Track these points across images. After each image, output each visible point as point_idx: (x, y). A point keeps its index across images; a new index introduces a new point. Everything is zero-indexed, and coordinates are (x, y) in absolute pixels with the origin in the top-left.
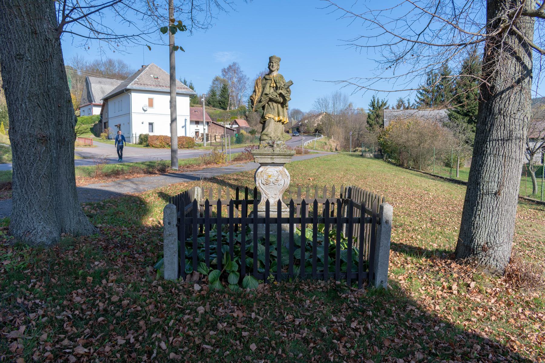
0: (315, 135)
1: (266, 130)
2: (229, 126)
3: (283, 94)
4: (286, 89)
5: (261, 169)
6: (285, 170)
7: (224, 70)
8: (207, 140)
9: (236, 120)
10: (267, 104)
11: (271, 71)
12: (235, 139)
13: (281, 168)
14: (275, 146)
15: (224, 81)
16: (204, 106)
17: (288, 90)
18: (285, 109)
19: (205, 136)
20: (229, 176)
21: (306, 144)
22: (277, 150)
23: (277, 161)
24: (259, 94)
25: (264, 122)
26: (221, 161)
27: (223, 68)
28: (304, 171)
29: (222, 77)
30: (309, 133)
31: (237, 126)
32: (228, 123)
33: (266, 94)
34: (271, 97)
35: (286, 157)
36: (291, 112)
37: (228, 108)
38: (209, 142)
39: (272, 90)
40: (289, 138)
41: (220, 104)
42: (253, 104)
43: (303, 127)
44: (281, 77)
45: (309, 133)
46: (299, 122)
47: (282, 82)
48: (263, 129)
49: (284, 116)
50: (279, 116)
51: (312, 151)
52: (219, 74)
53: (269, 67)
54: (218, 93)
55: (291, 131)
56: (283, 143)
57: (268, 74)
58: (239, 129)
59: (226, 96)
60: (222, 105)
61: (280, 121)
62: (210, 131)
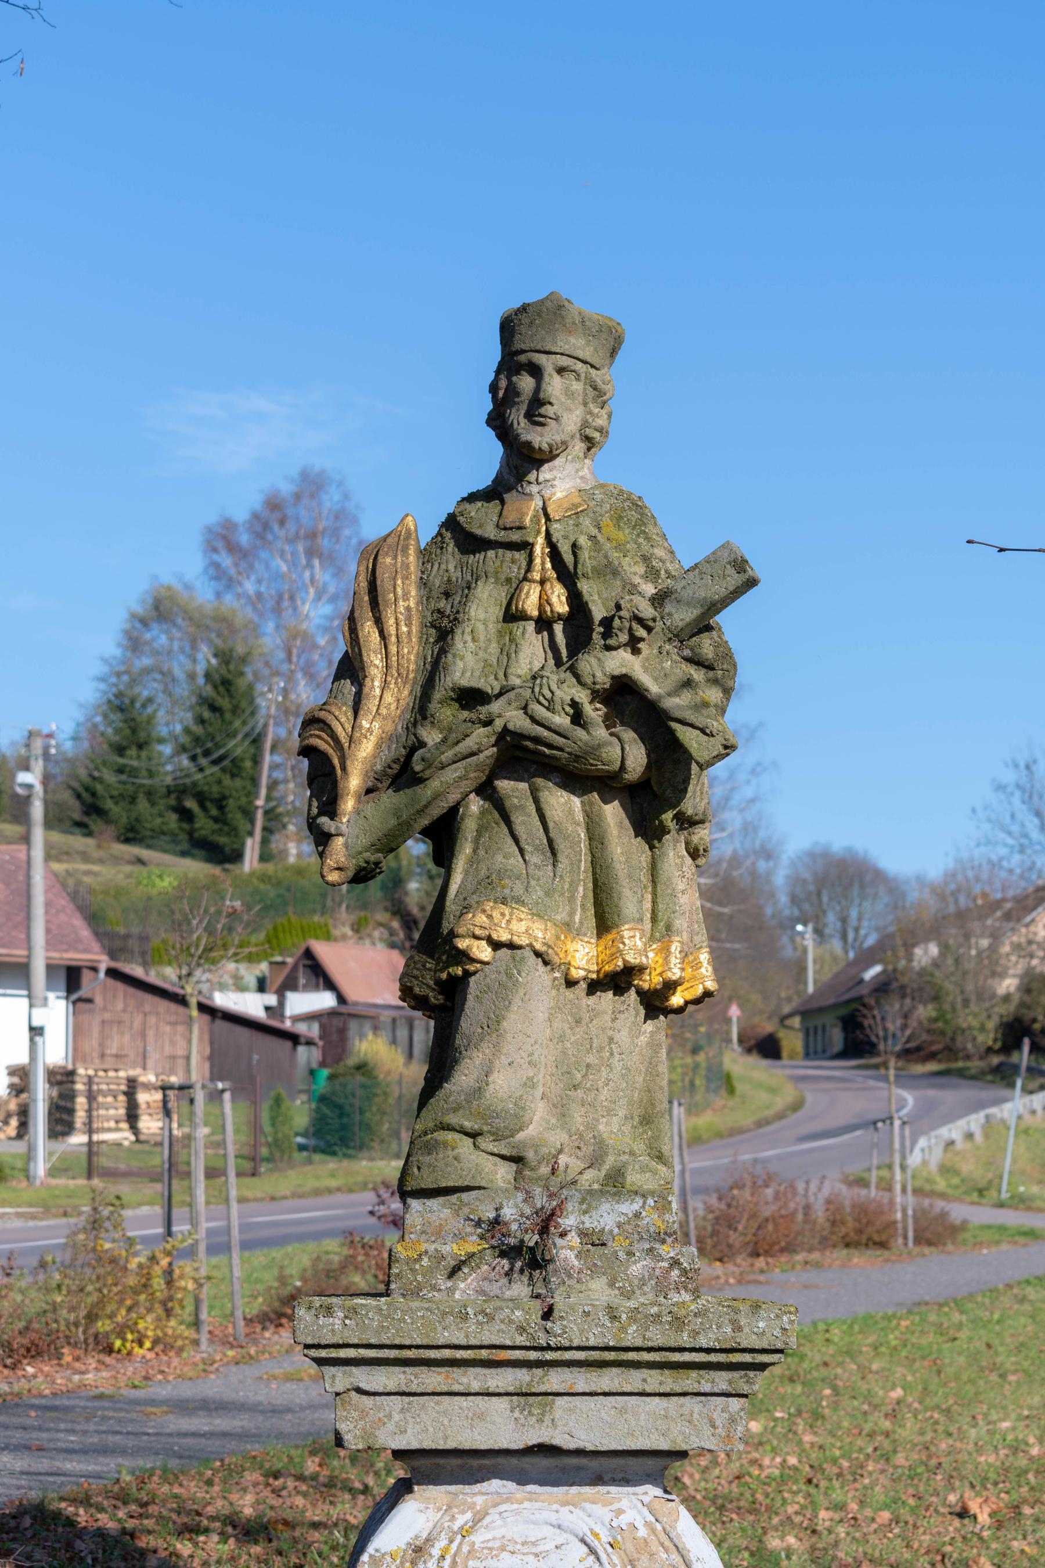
0: (1004, 1076)
1: (463, 1078)
2: (252, 1004)
3: (653, 687)
4: (680, 637)
5: (411, 1519)
6: (688, 1530)
7: (222, 538)
8: (61, 1121)
9: (323, 951)
10: (475, 805)
11: (522, 461)
12: (300, 1114)
13: (633, 1506)
14: (566, 1251)
15: (224, 622)
16: (38, 835)
17: (706, 646)
18: (674, 851)
19: (41, 1093)
20: (192, 1489)
21: (924, 1153)
22: (589, 1304)
23: (584, 1423)
24: (387, 699)
25: (442, 991)
26: (147, 1324)
27: (212, 518)
28: (908, 1430)
29: (204, 594)
30: (951, 1051)
31: (325, 1000)
32: (250, 975)
33: (470, 698)
34: (518, 721)
35: (690, 1381)
36: (796, 880)
37: (251, 848)
38: (78, 1139)
39: (532, 651)
40: (779, 1103)
41: (186, 815)
42: (330, 807)
43: (894, 1007)
44: (633, 514)
45: (951, 1051)
46: (868, 958)
47: (634, 570)
48: (442, 1062)
49: (661, 929)
50: (605, 923)
51: (980, 1215)
52: (185, 567)
53: (498, 422)
54: (171, 722)
55: (792, 1041)
56: (651, 1219)
57: (494, 493)
58: (336, 1026)
59: (237, 746)
60: (204, 825)
61: (617, 980)
62: (92, 1043)
